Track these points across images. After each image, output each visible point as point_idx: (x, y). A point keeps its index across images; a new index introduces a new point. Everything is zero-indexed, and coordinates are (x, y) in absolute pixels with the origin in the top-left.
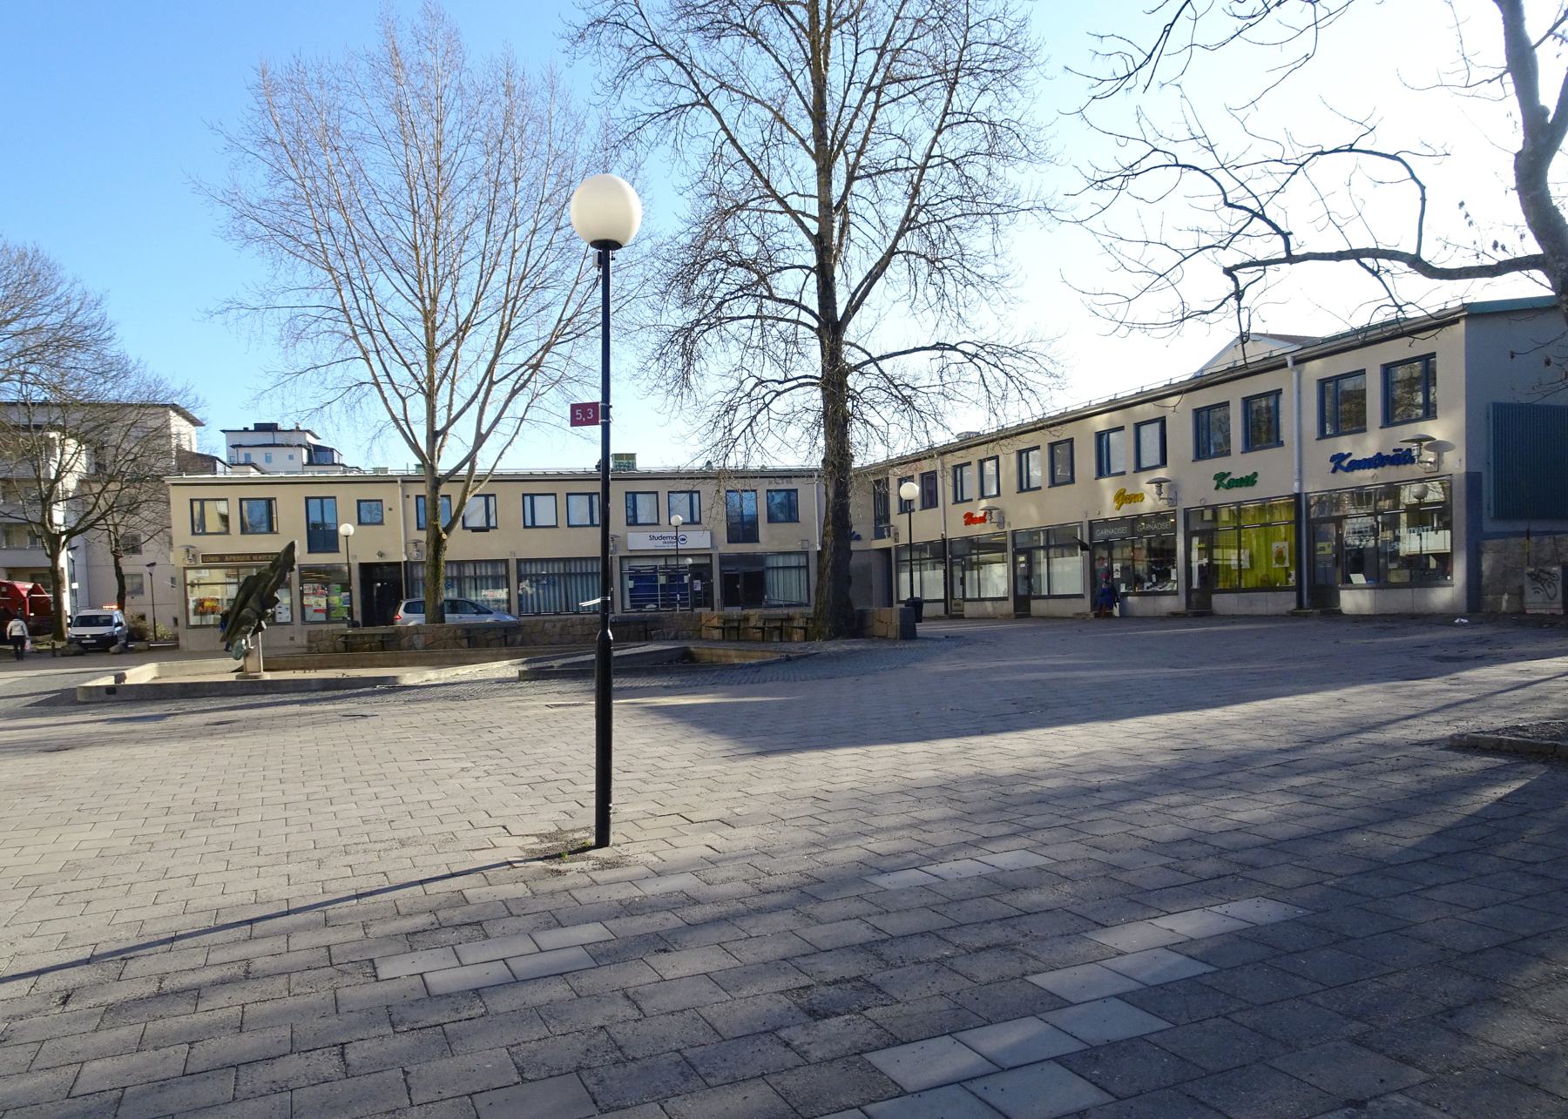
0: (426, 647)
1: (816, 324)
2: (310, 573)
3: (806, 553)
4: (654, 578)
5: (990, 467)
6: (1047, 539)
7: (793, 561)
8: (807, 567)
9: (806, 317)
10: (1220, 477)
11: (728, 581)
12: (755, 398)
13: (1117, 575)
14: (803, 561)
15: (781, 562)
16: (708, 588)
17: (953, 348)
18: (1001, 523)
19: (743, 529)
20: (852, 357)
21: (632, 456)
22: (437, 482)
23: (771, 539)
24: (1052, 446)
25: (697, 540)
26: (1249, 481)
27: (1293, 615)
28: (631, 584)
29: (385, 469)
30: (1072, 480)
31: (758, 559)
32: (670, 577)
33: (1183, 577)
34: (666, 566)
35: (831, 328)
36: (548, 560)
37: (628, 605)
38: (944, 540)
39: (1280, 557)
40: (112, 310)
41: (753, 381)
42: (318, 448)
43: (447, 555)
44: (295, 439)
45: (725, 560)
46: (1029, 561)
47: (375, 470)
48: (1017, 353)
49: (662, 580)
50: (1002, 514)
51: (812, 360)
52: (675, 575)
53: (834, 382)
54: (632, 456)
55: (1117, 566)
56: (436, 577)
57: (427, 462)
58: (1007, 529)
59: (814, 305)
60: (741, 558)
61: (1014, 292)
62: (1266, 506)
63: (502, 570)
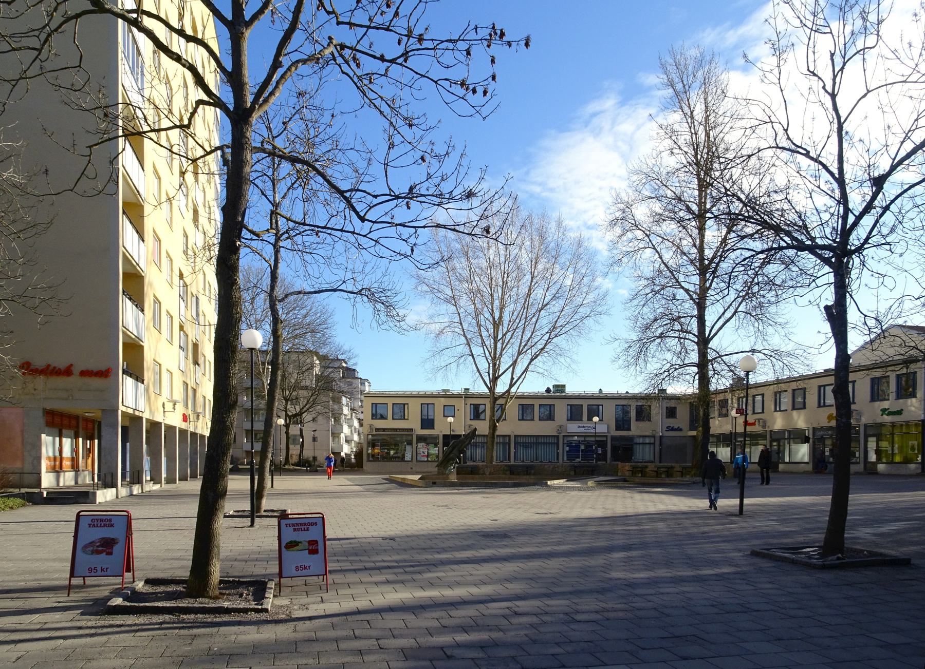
0: (658, 474)
1: (696, 340)
2: (421, 439)
3: (654, 437)
4: (578, 446)
5: (759, 398)
6: (789, 435)
7: (647, 440)
8: (654, 444)
9: (691, 337)
10: (884, 410)
11: (614, 448)
12: (671, 372)
13: (827, 454)
14: (652, 441)
15: (641, 440)
16: (605, 452)
17: (760, 352)
18: (764, 426)
19: (622, 423)
20: (711, 355)
21: (564, 386)
22: (496, 399)
23: (637, 429)
24: (794, 390)
25: (602, 429)
26: (899, 413)
27: (918, 475)
28: (567, 449)
29: (448, 391)
30: (804, 407)
31: (631, 439)
32: (586, 446)
33: (862, 456)
34: (585, 441)
35: (703, 342)
36: (547, 436)
37: (565, 459)
38: (731, 433)
39: (913, 448)
40: (336, 318)
41: (669, 365)
42: (348, 369)
43: (497, 433)
44: (336, 365)
45: (613, 438)
46: (779, 445)
47: (444, 391)
48: (789, 354)
49: (582, 447)
50: (765, 422)
51: (694, 357)
52: (588, 446)
53: (703, 365)
54: (564, 386)
55: (827, 449)
56: (493, 442)
57: (492, 389)
58: (767, 429)
59: (696, 331)
60: (622, 437)
61: (791, 330)
62: (907, 424)
63: (507, 440)
